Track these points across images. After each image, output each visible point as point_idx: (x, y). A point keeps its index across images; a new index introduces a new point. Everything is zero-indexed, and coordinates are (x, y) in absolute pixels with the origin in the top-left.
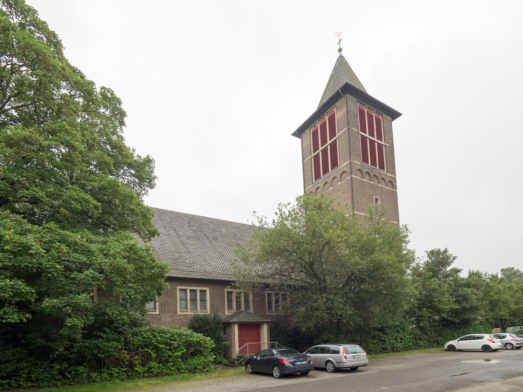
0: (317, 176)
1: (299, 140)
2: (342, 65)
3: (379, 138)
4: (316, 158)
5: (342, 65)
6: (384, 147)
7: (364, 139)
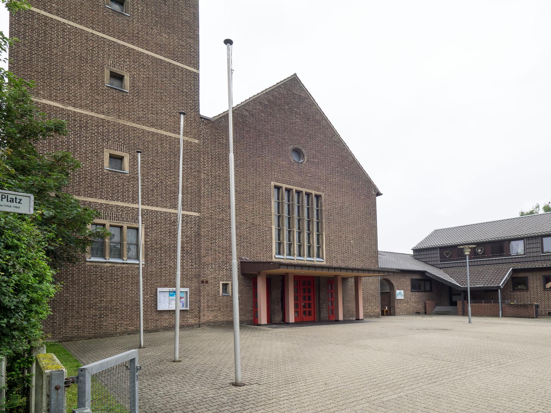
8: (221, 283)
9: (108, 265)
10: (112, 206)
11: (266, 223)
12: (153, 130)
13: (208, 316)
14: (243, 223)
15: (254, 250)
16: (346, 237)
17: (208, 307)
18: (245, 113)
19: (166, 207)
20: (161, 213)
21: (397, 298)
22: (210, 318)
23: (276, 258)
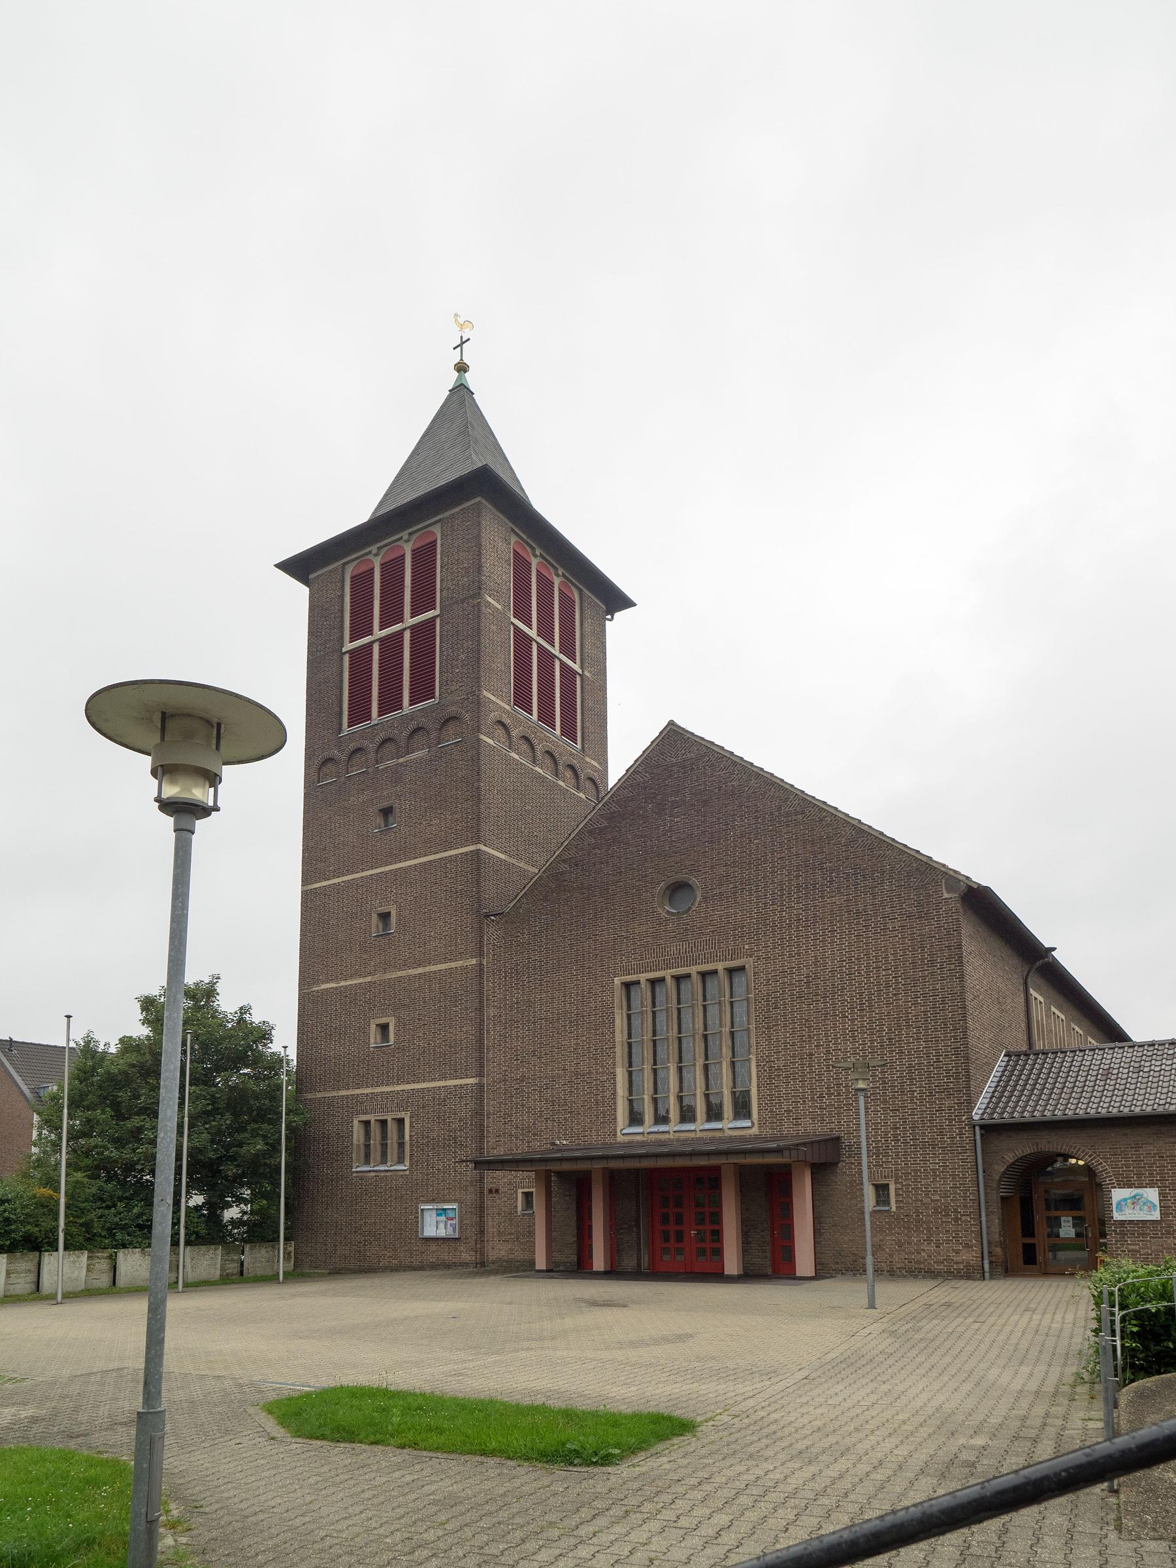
0: (360, 712)
1: (303, 592)
2: (459, 411)
3: (568, 648)
4: (423, 601)
5: (459, 411)
6: (578, 679)
7: (523, 641)
8: (520, 1191)
9: (373, 1174)
10: (377, 1095)
11: (603, 1066)
12: (420, 970)
13: (497, 1250)
14: (559, 1077)
15: (578, 1124)
16: (828, 1052)
17: (500, 1233)
18: (565, 867)
19: (433, 1080)
20: (429, 1090)
21: (1117, 1216)
22: (503, 1253)
23: (624, 1132)
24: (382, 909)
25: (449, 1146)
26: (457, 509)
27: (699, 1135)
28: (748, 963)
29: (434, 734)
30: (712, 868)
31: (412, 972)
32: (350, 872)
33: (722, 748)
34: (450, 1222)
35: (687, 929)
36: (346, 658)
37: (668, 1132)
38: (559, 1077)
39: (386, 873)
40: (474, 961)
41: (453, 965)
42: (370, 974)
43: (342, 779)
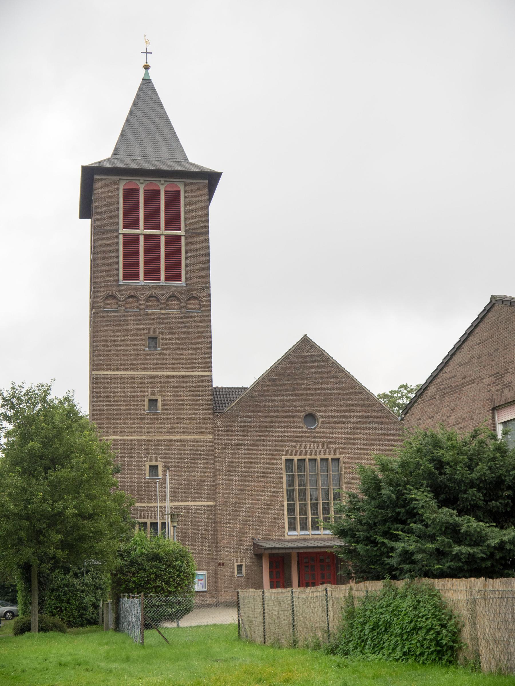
11: (277, 500)
12: (178, 437)
14: (255, 504)
15: (266, 529)
17: (225, 587)
18: (255, 394)
19: (188, 501)
20: (185, 507)
22: (227, 598)
24: (153, 397)
25: (198, 539)
26: (195, 181)
27: (322, 536)
28: (341, 457)
29: (183, 303)
30: (325, 410)
31: (173, 437)
32: (127, 370)
33: (328, 354)
34: (200, 582)
35: (315, 437)
36: (121, 237)
37: (309, 535)
38: (255, 504)
39: (154, 376)
40: (211, 437)
41: (198, 437)
42: (144, 434)
43: (122, 311)
